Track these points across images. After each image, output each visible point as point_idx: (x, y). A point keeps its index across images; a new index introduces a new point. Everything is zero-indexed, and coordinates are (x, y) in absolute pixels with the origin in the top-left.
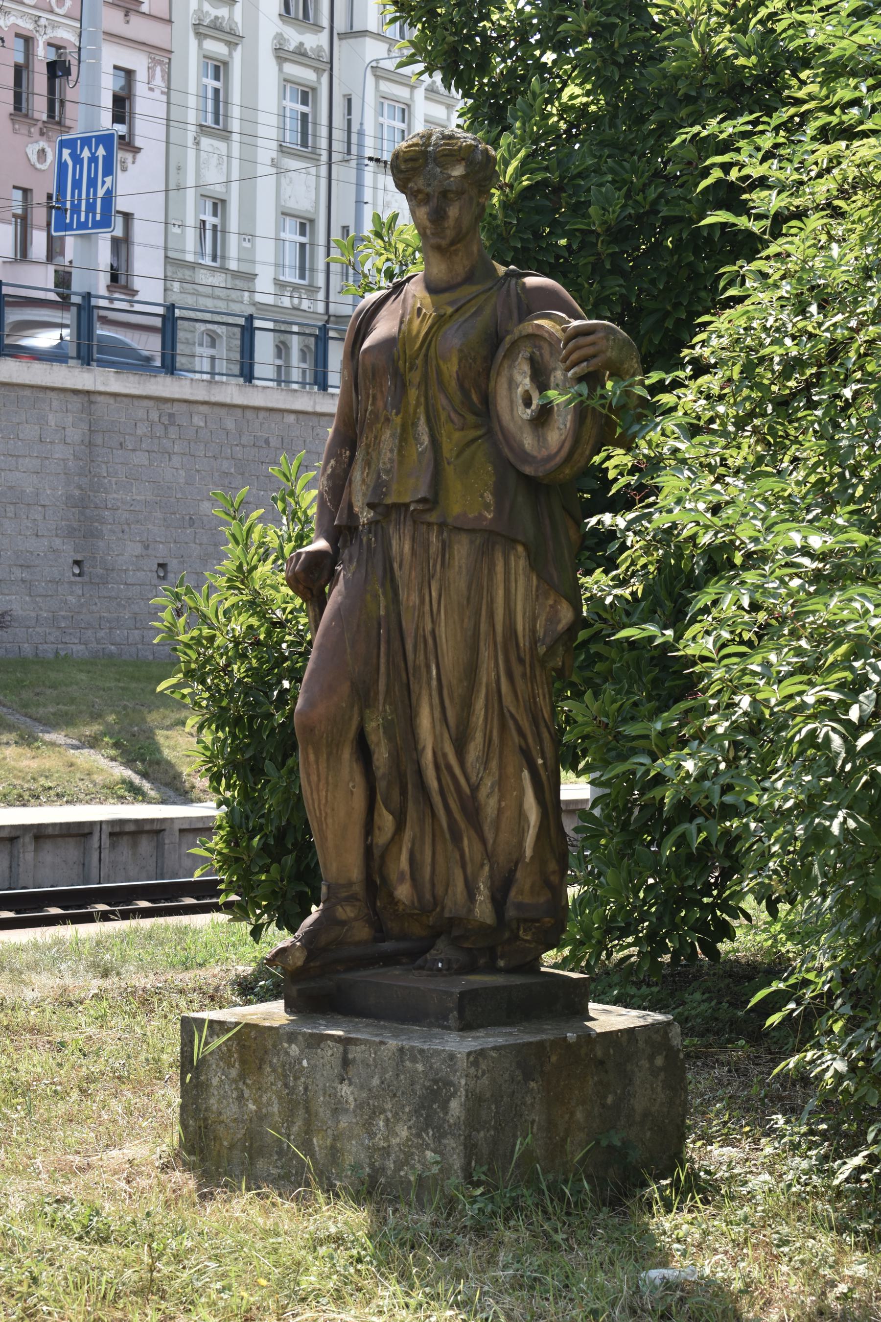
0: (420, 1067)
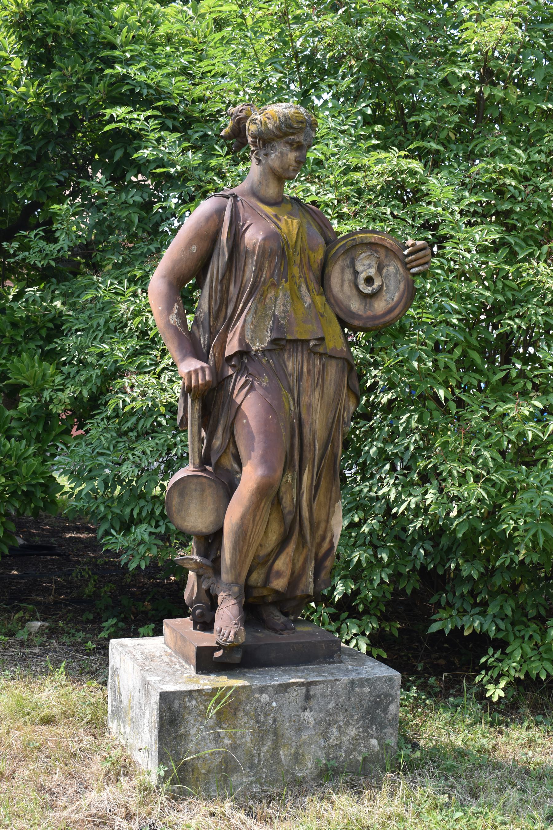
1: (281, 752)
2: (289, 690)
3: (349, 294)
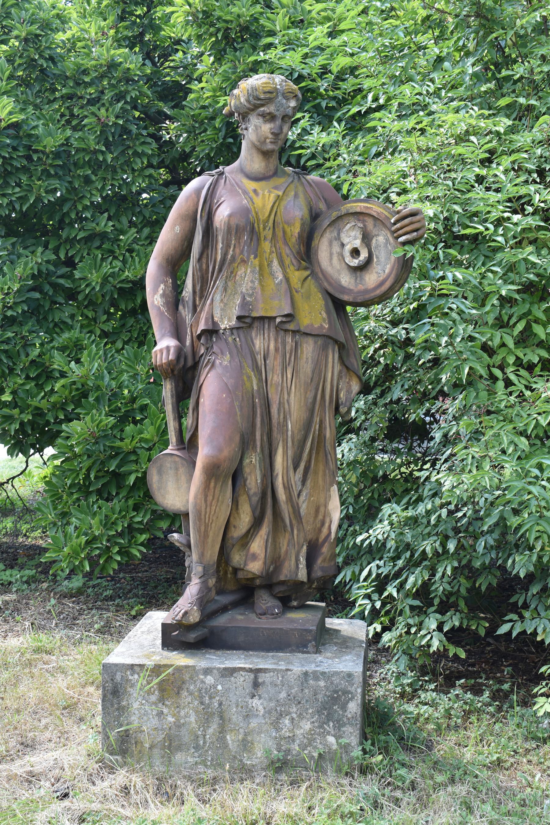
0: (322, 683)
1: (228, 737)
2: (235, 675)
3: (338, 267)
